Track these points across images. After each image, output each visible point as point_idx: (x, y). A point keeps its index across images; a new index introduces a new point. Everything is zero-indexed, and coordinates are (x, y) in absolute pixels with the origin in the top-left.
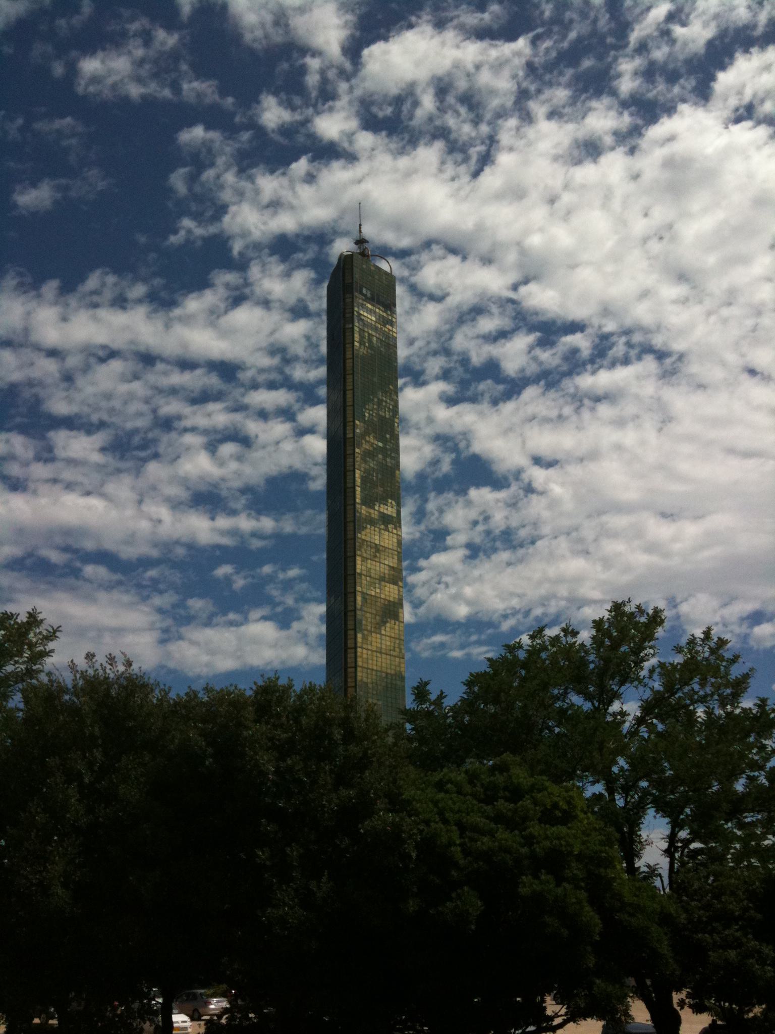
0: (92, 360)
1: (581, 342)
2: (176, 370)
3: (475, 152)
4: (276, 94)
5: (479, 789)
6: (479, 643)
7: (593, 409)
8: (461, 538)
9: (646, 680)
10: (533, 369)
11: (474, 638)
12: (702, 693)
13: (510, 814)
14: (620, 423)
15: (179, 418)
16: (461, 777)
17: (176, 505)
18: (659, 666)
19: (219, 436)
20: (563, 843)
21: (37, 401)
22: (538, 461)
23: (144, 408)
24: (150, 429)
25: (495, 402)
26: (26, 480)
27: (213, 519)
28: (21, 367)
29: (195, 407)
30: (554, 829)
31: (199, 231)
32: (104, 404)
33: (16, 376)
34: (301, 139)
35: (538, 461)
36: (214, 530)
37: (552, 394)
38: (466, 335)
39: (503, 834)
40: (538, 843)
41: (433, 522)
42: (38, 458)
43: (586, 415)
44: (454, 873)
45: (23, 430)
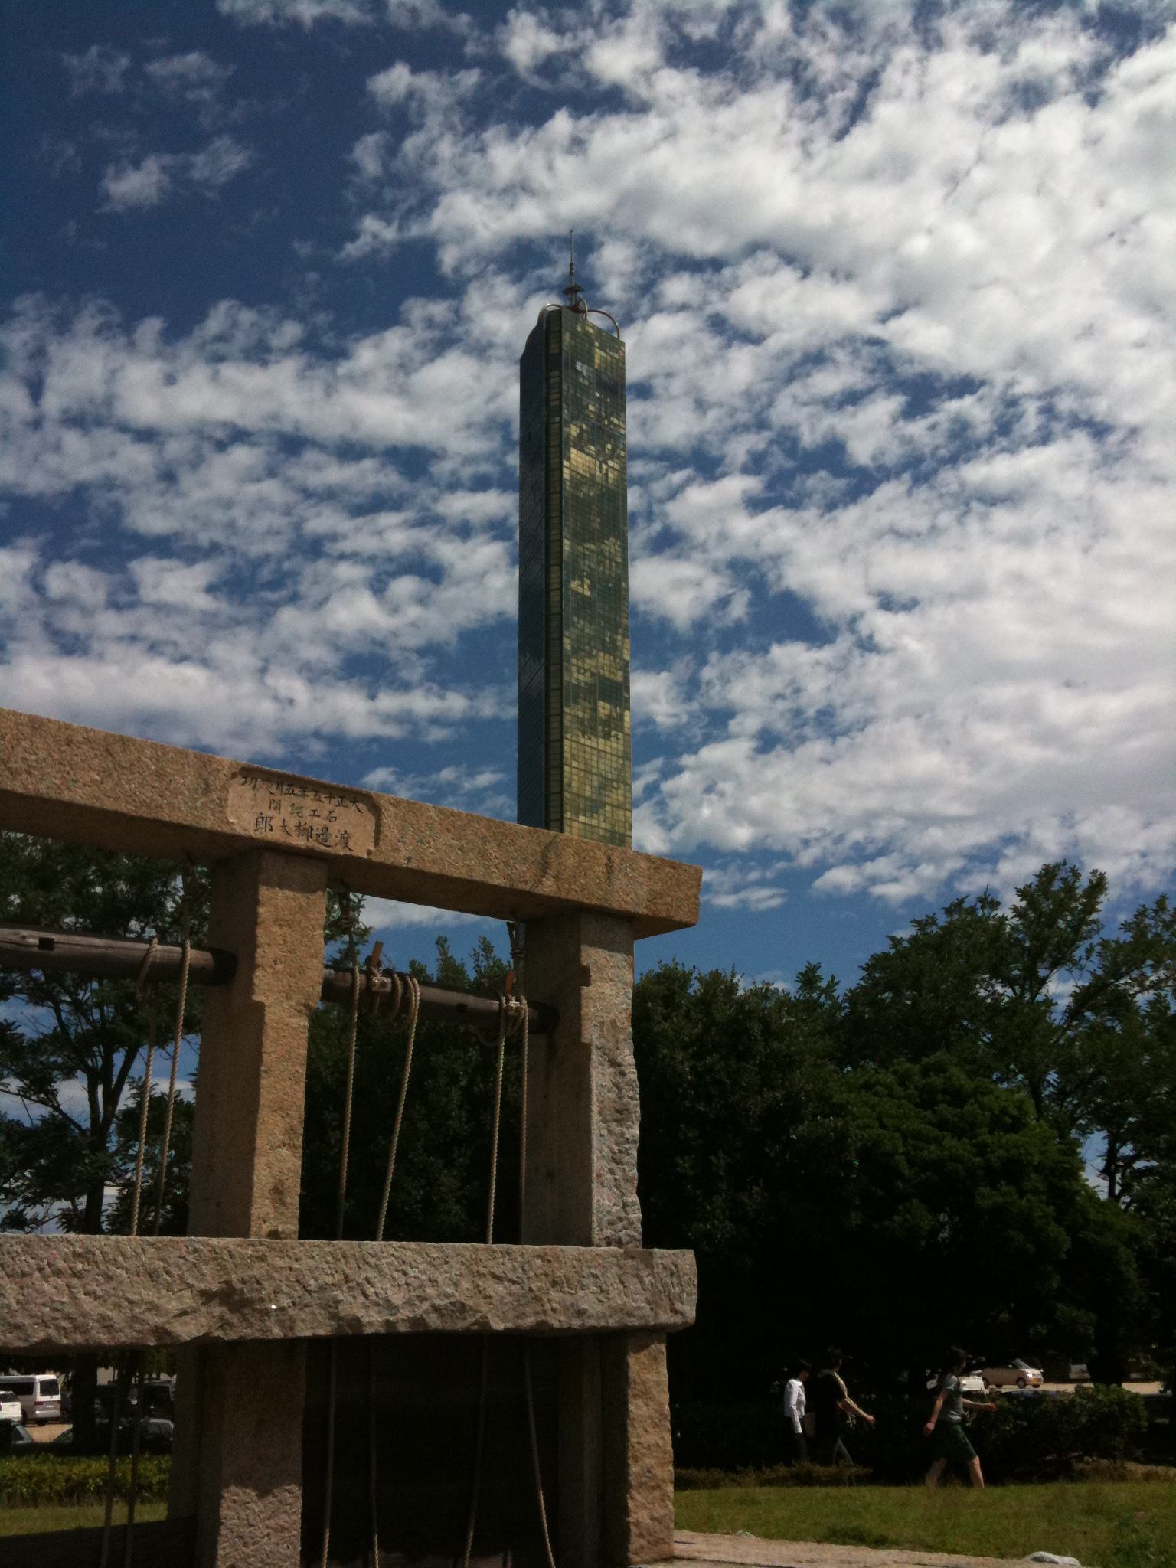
0: (207, 448)
1: (976, 410)
2: (333, 461)
3: (838, 101)
4: (531, 9)
5: (911, 1091)
6: (762, 883)
7: (984, 517)
8: (751, 723)
9: (1083, 962)
10: (894, 453)
11: (754, 876)
12: (1154, 978)
13: (955, 1119)
14: (1023, 540)
15: (334, 537)
16: (890, 1079)
17: (313, 674)
18: (1101, 944)
19: (391, 567)
20: (1022, 1151)
21: (118, 509)
22: (887, 603)
23: (279, 521)
24: (288, 557)
25: (831, 506)
26: (89, 636)
27: (372, 697)
28: (95, 458)
29: (360, 521)
30: (1008, 1136)
31: (389, 234)
32: (219, 516)
33: (87, 473)
34: (569, 81)
35: (887, 603)
36: (372, 713)
37: (923, 492)
38: (795, 398)
39: (950, 1141)
40: (993, 1152)
41: (715, 697)
42: (115, 605)
43: (973, 526)
44: (900, 1185)
45: (89, 559)
